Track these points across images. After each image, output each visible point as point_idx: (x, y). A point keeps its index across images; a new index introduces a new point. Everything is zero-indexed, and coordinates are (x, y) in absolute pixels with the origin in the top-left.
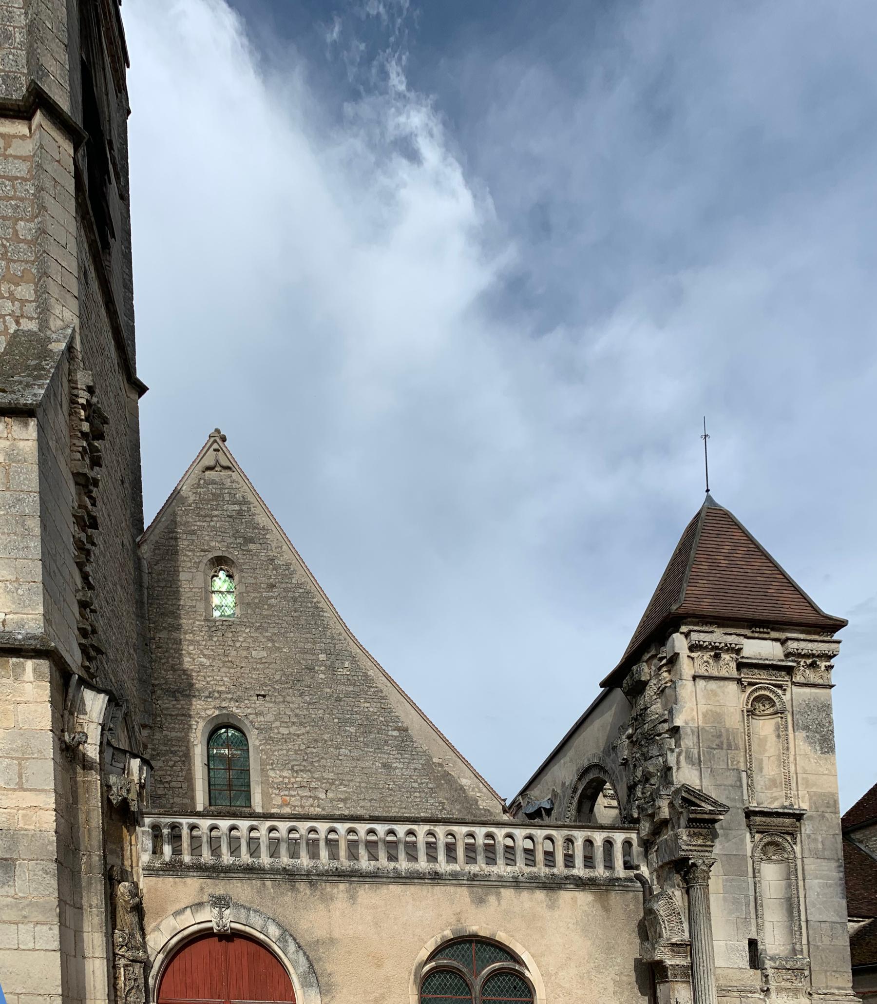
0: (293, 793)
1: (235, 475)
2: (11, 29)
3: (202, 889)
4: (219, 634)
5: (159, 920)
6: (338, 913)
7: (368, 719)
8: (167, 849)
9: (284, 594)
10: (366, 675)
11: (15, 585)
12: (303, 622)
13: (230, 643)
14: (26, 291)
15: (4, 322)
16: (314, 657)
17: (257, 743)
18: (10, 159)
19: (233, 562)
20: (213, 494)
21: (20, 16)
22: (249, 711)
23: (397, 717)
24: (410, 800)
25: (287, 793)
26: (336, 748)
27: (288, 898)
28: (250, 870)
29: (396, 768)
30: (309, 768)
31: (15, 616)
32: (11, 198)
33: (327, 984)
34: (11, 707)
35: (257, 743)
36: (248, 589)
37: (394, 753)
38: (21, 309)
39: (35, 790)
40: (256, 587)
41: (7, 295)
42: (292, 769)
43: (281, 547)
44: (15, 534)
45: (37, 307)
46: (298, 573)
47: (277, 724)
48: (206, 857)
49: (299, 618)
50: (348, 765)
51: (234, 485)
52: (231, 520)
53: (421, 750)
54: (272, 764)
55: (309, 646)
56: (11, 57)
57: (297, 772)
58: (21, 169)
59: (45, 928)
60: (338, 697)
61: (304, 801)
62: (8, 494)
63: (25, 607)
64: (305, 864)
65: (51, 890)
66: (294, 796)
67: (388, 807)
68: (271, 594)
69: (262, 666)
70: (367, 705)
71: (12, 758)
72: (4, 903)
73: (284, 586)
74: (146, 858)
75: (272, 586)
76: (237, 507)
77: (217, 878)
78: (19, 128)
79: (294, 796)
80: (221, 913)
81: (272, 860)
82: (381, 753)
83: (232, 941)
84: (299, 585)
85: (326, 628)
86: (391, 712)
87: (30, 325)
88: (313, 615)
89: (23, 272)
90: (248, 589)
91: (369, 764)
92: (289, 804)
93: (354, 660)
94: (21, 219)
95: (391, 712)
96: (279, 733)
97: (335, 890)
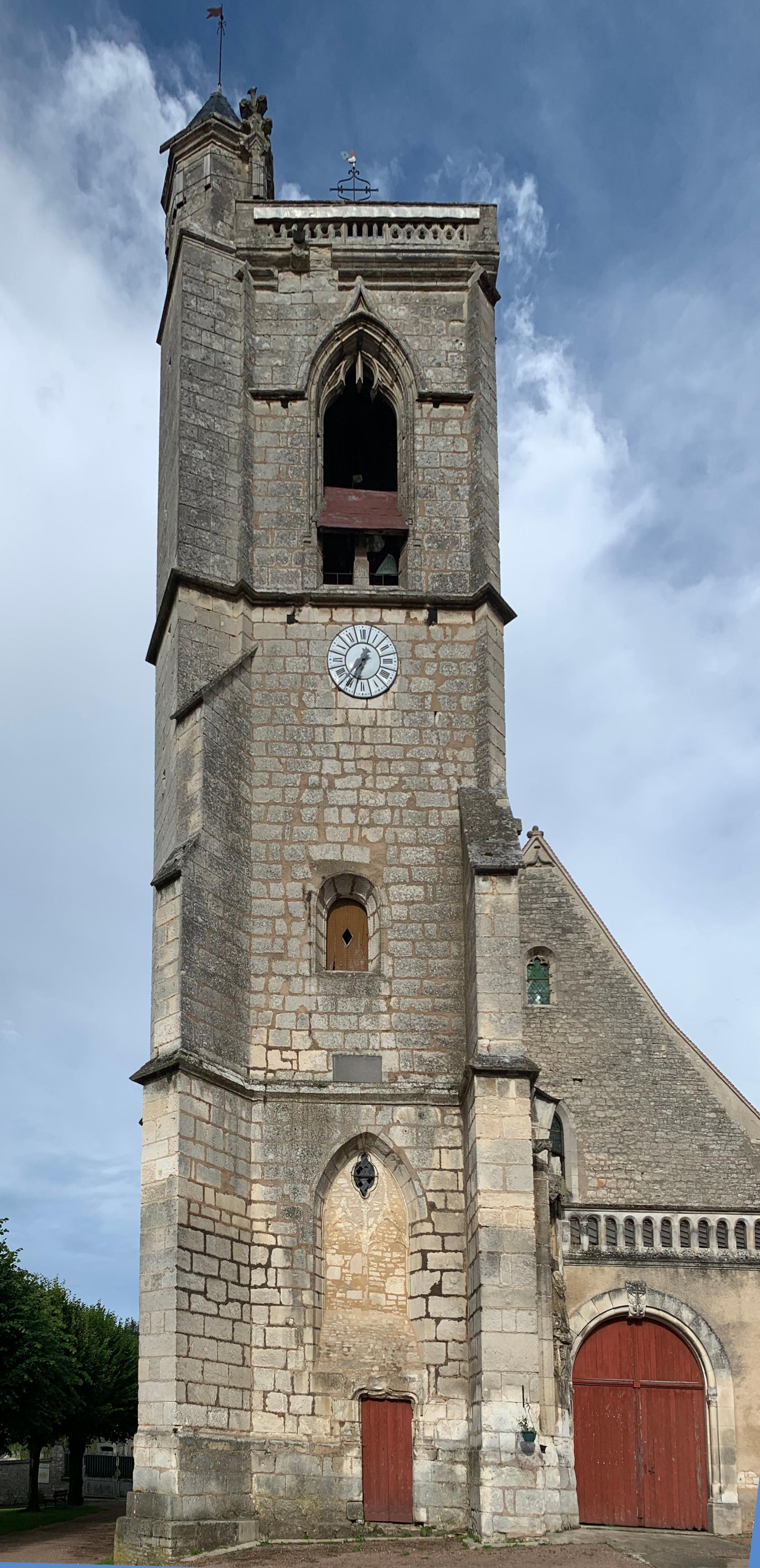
0: (609, 1175)
1: (555, 870)
2: (458, 535)
3: (619, 1276)
4: (537, 1021)
5: (578, 1305)
6: (747, 1299)
7: (684, 1101)
8: (585, 1240)
9: (601, 981)
10: (683, 1059)
11: (499, 1015)
12: (619, 1007)
13: (548, 1030)
14: (467, 754)
15: (448, 782)
16: (630, 1042)
17: (574, 1126)
18: (457, 645)
19: (551, 952)
20: (533, 889)
21: (465, 524)
22: (566, 1095)
23: (714, 1099)
24: (727, 1181)
25: (602, 1175)
26: (652, 1131)
27: (700, 1284)
28: (665, 1259)
29: (713, 1150)
30: (625, 1150)
31: (499, 1042)
32: (457, 677)
33: (738, 1366)
34: (497, 1120)
35: (574, 1126)
36: (566, 977)
37: (711, 1134)
38: (463, 770)
39: (518, 1192)
40: (573, 975)
41: (451, 759)
42: (609, 1152)
43: (599, 936)
44: (499, 973)
45: (477, 767)
46: (615, 959)
47: (594, 1107)
48: (622, 1246)
49: (615, 1003)
50: (664, 1148)
51: (554, 879)
52: (550, 912)
53: (739, 1131)
54: (588, 1147)
55: (625, 1030)
56: (457, 558)
57: (613, 1154)
58: (464, 652)
59: (525, 1313)
60: (655, 1080)
61: (620, 1183)
62: (493, 939)
63: (506, 1034)
64: (715, 1253)
65: (531, 1280)
66: (610, 1178)
67: (704, 1189)
68: (588, 981)
69: (578, 1051)
70: (683, 1087)
71: (497, 1164)
72: (490, 1291)
73: (601, 972)
74: (566, 1247)
75: (589, 973)
76: (556, 900)
77: (634, 1266)
78: (465, 618)
79: (610, 1178)
80: (638, 1299)
81: (683, 1249)
82: (698, 1135)
83: (641, 1325)
84: (616, 972)
85: (642, 1013)
86: (708, 1094)
87: (469, 783)
88: (630, 1000)
89: (465, 738)
90: (566, 977)
91: (686, 1146)
92: (605, 1186)
93: (670, 1042)
94: (464, 694)
95: (708, 1094)
96: (595, 1116)
97: (745, 1277)
